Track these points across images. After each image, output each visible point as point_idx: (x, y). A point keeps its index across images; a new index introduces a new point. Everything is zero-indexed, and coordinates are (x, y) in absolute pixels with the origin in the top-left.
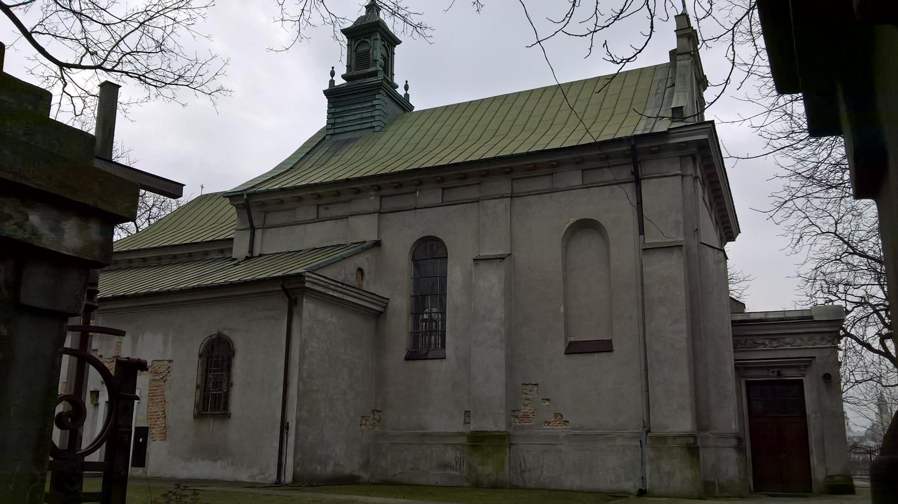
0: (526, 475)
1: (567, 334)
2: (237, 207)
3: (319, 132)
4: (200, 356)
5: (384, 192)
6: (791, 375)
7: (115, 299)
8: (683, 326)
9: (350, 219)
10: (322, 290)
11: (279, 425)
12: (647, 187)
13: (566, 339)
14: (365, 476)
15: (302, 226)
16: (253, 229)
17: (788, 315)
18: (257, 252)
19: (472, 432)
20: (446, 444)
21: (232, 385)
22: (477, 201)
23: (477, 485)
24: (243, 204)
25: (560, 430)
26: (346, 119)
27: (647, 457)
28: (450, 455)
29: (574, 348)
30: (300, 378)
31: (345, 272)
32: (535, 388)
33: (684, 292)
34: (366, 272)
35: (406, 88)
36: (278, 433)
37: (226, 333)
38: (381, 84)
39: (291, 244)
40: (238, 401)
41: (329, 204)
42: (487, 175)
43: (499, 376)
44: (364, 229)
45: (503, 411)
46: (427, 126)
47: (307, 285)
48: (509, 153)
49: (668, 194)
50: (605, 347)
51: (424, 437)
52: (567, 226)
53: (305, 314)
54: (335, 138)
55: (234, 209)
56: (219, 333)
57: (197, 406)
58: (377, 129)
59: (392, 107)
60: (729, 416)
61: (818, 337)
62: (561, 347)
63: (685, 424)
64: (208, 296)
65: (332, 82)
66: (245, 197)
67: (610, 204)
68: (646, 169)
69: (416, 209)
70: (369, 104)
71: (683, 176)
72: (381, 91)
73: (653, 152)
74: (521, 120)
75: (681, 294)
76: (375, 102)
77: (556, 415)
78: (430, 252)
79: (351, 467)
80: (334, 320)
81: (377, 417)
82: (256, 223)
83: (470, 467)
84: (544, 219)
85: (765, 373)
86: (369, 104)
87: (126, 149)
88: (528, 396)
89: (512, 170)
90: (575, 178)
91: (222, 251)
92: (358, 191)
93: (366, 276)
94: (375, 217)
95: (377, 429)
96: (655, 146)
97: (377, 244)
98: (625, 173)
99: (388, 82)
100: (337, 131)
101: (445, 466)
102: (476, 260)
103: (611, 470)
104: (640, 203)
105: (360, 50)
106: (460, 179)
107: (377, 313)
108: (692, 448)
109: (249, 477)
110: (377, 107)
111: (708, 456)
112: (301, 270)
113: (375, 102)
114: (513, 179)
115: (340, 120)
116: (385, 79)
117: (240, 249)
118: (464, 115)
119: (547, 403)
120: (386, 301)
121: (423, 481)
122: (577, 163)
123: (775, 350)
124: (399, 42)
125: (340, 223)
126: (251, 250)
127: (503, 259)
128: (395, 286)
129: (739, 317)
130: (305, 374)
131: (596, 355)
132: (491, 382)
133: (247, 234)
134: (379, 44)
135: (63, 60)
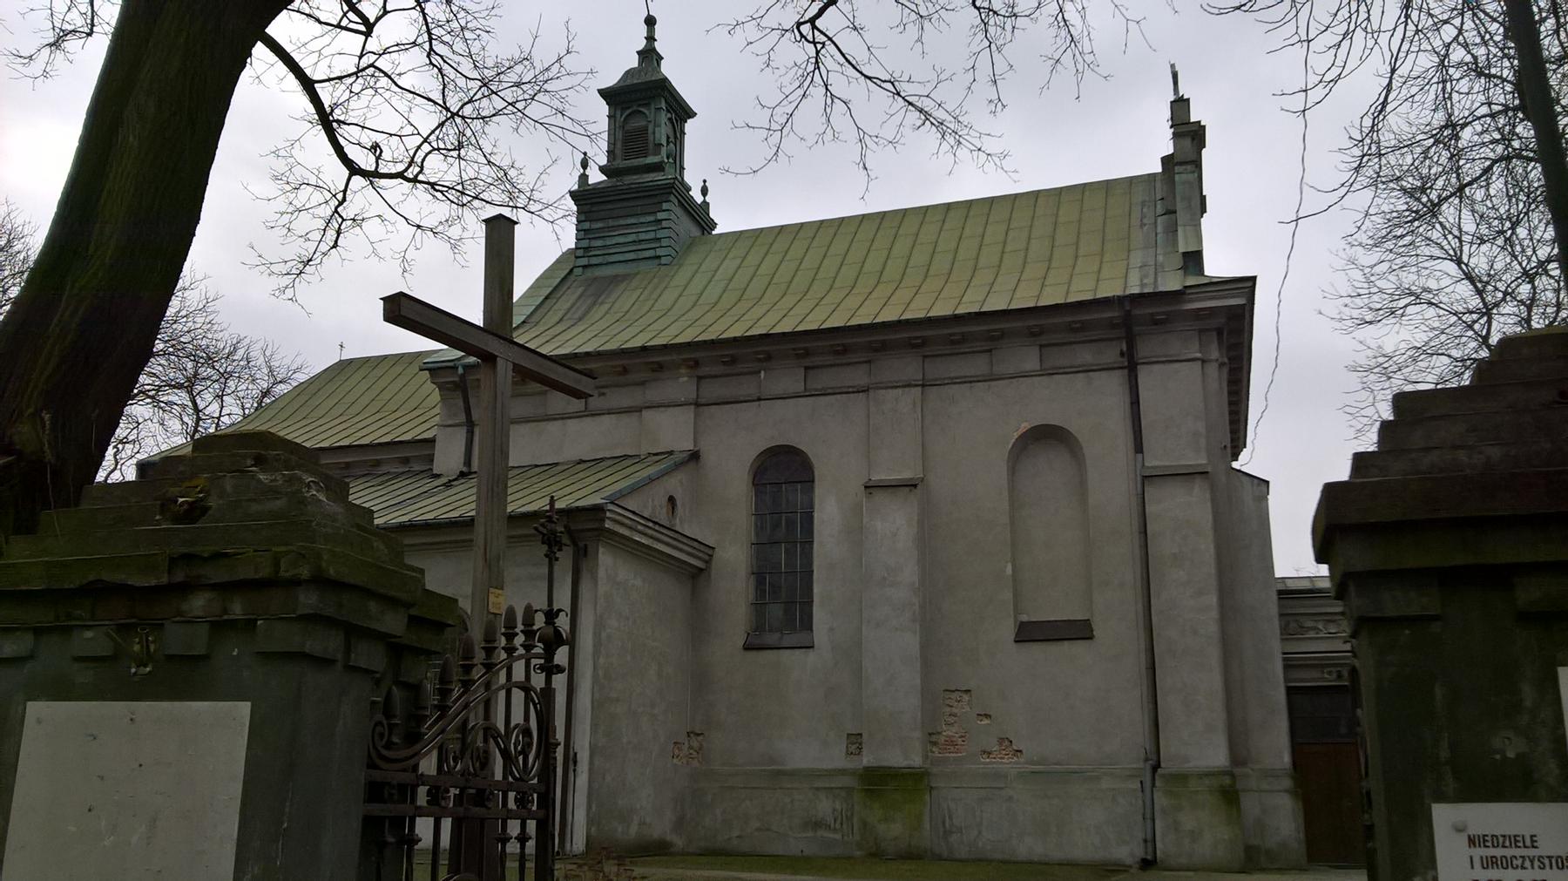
0: (954, 838)
1: (1017, 611)
2: (441, 387)
3: (558, 261)
5: (705, 370)
8: (1213, 599)
9: (646, 414)
10: (626, 532)
12: (1148, 378)
14: (679, 842)
19: (867, 769)
20: (817, 789)
22: (865, 390)
23: (877, 855)
24: (1112, 325)
25: (1007, 764)
26: (609, 242)
28: (825, 807)
29: (1029, 633)
31: (651, 504)
32: (966, 697)
35: (704, 191)
42: (884, 347)
44: (672, 430)
45: (917, 734)
46: (752, 260)
49: (1176, 386)
50: (1080, 631)
51: (779, 776)
52: (1016, 435)
53: (601, 573)
54: (589, 273)
58: (664, 261)
59: (685, 226)
60: (1275, 745)
62: (1008, 630)
63: (1216, 756)
64: (429, 540)
66: (460, 370)
67: (1087, 402)
68: (1144, 349)
69: (759, 399)
70: (651, 218)
71: (1203, 361)
72: (672, 198)
73: (1156, 323)
74: (920, 258)
75: (1206, 546)
76: (660, 216)
77: (1001, 740)
78: (783, 474)
79: (661, 828)
80: (638, 582)
81: (695, 744)
83: (865, 824)
84: (978, 424)
85: (1315, 674)
86: (651, 218)
87: (199, 277)
88: (954, 710)
89: (924, 342)
90: (1029, 359)
92: (660, 367)
94: (688, 414)
95: (695, 763)
97: (695, 456)
98: (1111, 353)
100: (594, 261)
101: (817, 825)
103: (1097, 828)
104: (1135, 403)
106: (837, 353)
108: (1230, 795)
110: (664, 224)
111: (1250, 804)
112: (596, 500)
113: (660, 216)
115: (599, 243)
117: (449, 457)
118: (815, 244)
119: (986, 721)
121: (778, 849)
122: (1033, 335)
124: (692, 114)
127: (915, 486)
128: (728, 530)
130: (601, 673)
132: (896, 686)
133: (461, 434)
134: (663, 117)
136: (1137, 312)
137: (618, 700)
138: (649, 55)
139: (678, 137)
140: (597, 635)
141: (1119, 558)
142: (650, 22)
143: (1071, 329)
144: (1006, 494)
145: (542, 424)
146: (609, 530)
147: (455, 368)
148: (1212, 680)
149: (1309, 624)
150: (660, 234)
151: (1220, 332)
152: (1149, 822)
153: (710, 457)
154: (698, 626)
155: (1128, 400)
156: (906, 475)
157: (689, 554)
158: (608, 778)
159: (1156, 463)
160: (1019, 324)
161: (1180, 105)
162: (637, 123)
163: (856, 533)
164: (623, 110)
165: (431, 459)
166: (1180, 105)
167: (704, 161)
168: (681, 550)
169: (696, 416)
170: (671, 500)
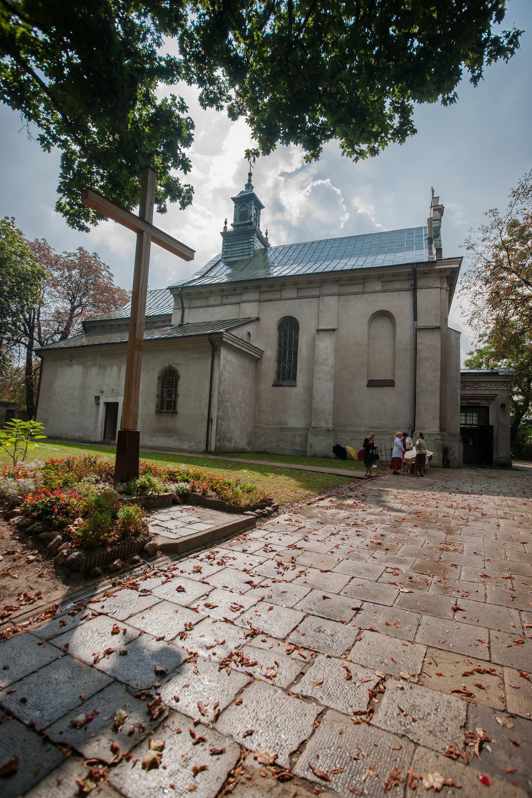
2: (174, 296)
4: (159, 378)
5: (262, 289)
6: (483, 403)
8: (439, 374)
11: (206, 419)
16: (183, 309)
21: (178, 395)
24: (409, 274)
29: (372, 384)
30: (219, 393)
34: (252, 335)
35: (267, 234)
36: (205, 423)
37: (174, 366)
40: (182, 404)
44: (250, 310)
45: (331, 417)
50: (390, 383)
53: (222, 356)
55: (172, 296)
56: (170, 366)
57: (157, 406)
61: (500, 384)
62: (365, 382)
65: (225, 228)
67: (399, 303)
68: (419, 283)
71: (441, 288)
75: (438, 355)
76: (251, 240)
78: (289, 327)
79: (242, 444)
80: (236, 361)
82: (185, 305)
90: (378, 286)
91: (164, 321)
97: (258, 319)
98: (407, 285)
100: (228, 256)
105: (241, 210)
106: (309, 283)
107: (255, 359)
109: (189, 447)
113: (251, 240)
114: (261, 292)
115: (230, 250)
123: (476, 389)
125: (235, 306)
126: (182, 320)
128: (266, 341)
131: (385, 388)
134: (253, 207)
135: (102, 616)
137: (227, 401)
138: (249, 186)
139: (258, 214)
141: (405, 359)
142: (250, 175)
143: (394, 275)
144: (367, 334)
146: (224, 342)
147: (178, 288)
148: (436, 401)
149: (468, 384)
151: (447, 277)
152: (214, 415)
153: (263, 320)
154: (257, 378)
156: (332, 327)
158: (223, 427)
159: (421, 325)
161: (435, 199)
163: (313, 348)
165: (170, 320)
166: (435, 199)
167: (266, 222)
170: (249, 334)
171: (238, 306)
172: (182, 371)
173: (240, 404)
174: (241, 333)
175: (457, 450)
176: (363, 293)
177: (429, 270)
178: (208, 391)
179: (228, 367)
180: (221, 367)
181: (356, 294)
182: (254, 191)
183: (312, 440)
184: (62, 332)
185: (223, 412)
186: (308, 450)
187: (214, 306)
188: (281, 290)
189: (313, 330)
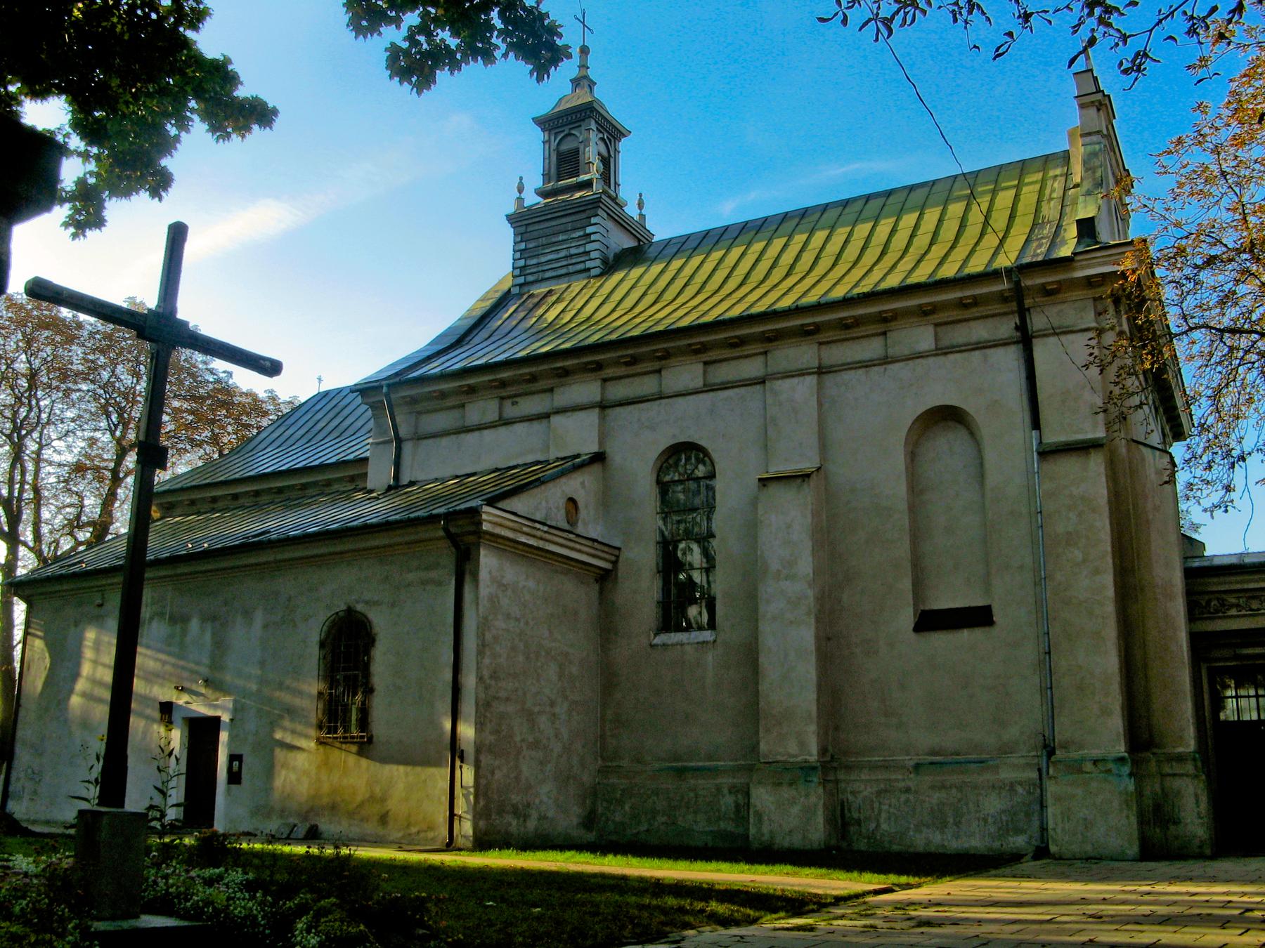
4: (322, 645)
7: (174, 560)
8: (1108, 579)
9: (555, 419)
10: (510, 534)
13: (915, 605)
15: (477, 434)
17: (1247, 560)
18: (405, 480)
22: (762, 381)
24: (1003, 298)
26: (543, 259)
27: (1049, 794)
29: (929, 621)
30: (480, 679)
33: (1107, 522)
34: (581, 504)
37: (360, 607)
38: (599, 200)
39: (449, 462)
41: (516, 396)
42: (565, 373)
43: (807, 671)
45: (813, 728)
47: (486, 526)
48: (763, 309)
50: (980, 617)
53: (484, 574)
58: (594, 272)
62: (907, 618)
65: (520, 200)
67: (986, 380)
68: (1037, 321)
69: (661, 398)
72: (600, 212)
76: (589, 230)
80: (531, 584)
90: (922, 337)
93: (583, 513)
96: (1053, 283)
97: (599, 458)
99: (610, 197)
100: (530, 278)
102: (764, 482)
105: (565, 147)
106: (627, 364)
110: (593, 237)
113: (589, 230)
114: (605, 380)
115: (534, 261)
116: (604, 192)
117: (379, 475)
120: (616, 552)
125: (537, 426)
126: (397, 477)
129: (1196, 563)
130: (486, 674)
134: (594, 136)
136: (1027, 282)
140: (481, 635)
143: (961, 304)
145: (463, 436)
146: (487, 533)
150: (588, 247)
153: (617, 456)
155: (1023, 375)
157: (588, 554)
158: (498, 775)
160: (576, 361)
162: (567, 146)
163: (752, 529)
164: (556, 134)
168: (579, 551)
169: (602, 419)
171: (545, 422)
172: (379, 620)
173: (552, 704)
174: (544, 503)
175: (1193, 808)
176: (886, 361)
177: (1059, 282)
178: (448, 675)
179: (505, 602)
180: (484, 603)
181: (866, 365)
182: (598, 93)
183: (763, 797)
184: (92, 523)
185: (496, 732)
186: (752, 831)
187: (480, 428)
188: (659, 371)
189: (753, 480)
